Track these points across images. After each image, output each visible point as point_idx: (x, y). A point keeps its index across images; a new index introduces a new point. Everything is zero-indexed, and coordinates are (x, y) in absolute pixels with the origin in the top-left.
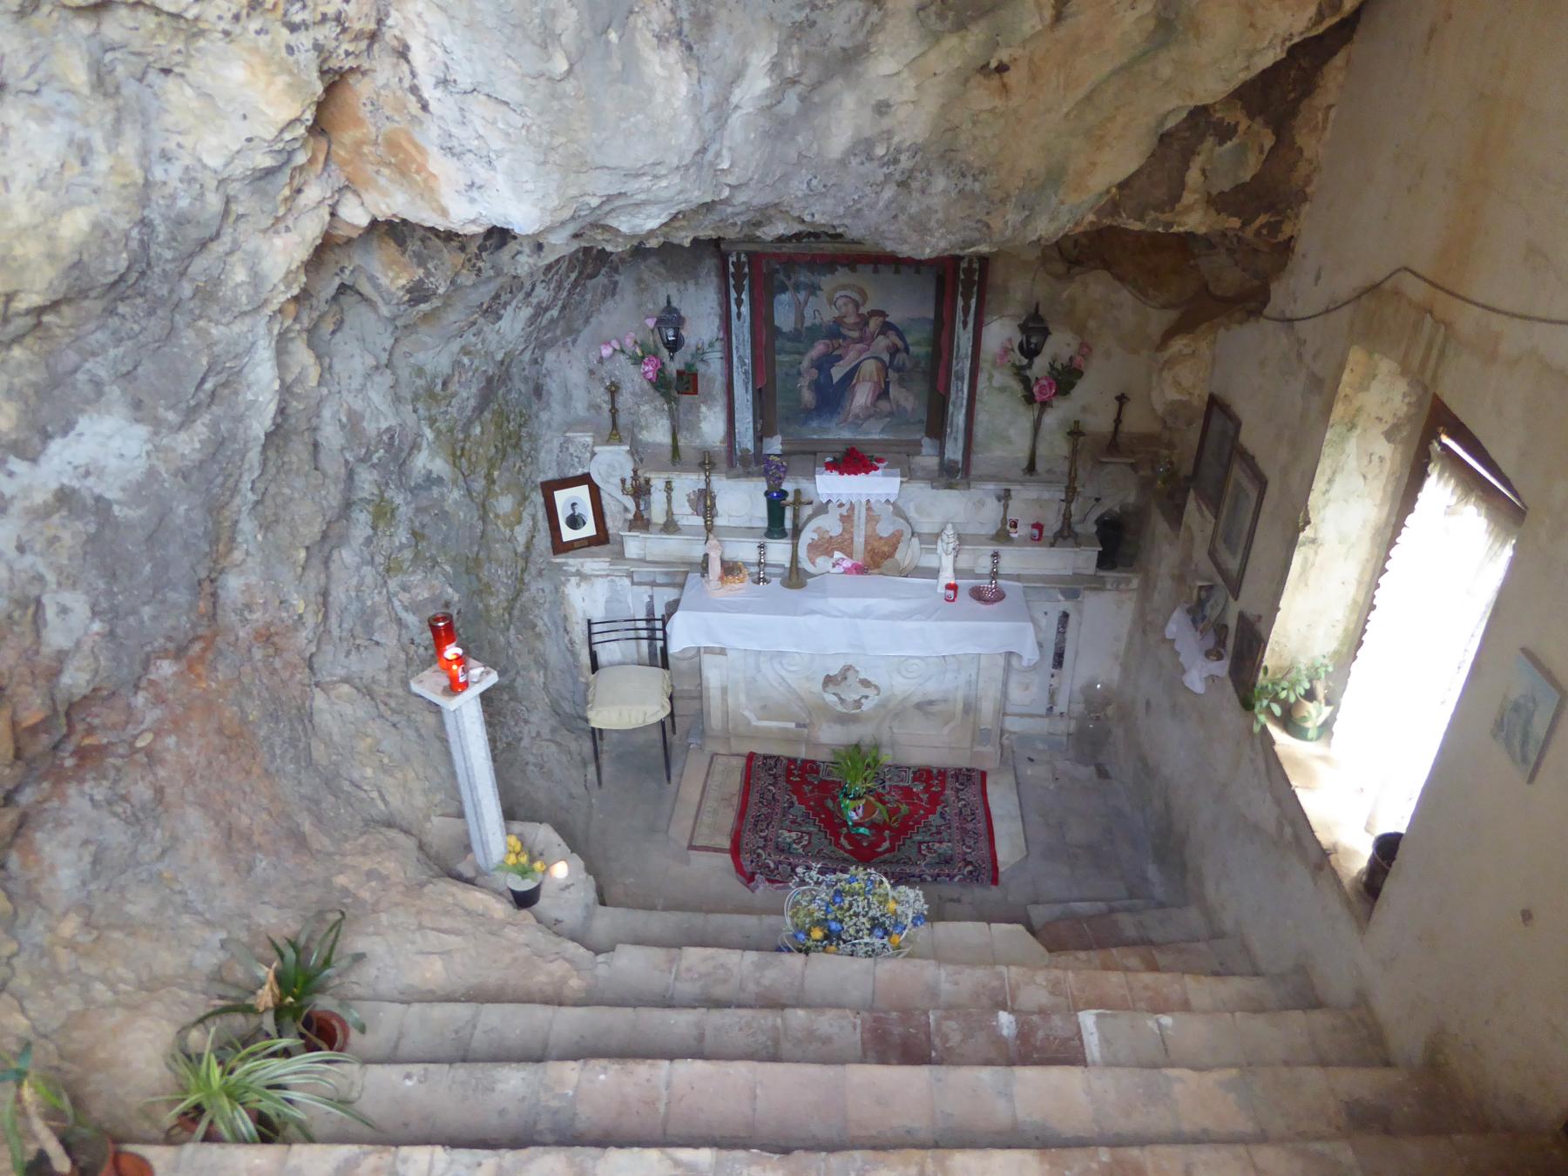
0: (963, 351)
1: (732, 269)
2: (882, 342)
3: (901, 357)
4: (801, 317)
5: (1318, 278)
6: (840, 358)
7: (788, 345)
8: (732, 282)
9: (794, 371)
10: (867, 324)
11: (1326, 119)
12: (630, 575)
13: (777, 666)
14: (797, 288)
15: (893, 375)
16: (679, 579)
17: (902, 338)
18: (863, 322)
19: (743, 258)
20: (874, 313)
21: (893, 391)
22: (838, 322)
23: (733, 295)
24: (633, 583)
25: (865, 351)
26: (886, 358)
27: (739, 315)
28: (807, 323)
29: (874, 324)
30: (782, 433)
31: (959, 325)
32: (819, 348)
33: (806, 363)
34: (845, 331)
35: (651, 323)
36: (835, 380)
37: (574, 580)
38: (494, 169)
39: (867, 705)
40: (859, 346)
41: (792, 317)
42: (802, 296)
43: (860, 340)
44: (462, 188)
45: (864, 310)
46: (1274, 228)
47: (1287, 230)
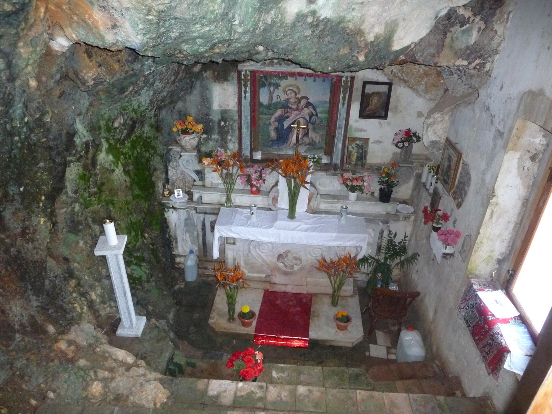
0: (342, 117)
1: (243, 77)
2: (306, 111)
3: (314, 118)
4: (271, 98)
5: (502, 88)
6: (288, 117)
7: (265, 111)
8: (243, 83)
9: (268, 122)
10: (300, 102)
11: (508, 18)
12: (195, 209)
13: (257, 250)
14: (270, 85)
15: (310, 126)
16: (216, 211)
17: (315, 110)
18: (299, 101)
19: (248, 73)
20: (303, 98)
21: (311, 133)
22: (287, 100)
23: (243, 88)
24: (197, 213)
25: (299, 114)
26: (308, 118)
27: (245, 97)
28: (274, 100)
29: (303, 102)
30: (261, 150)
31: (340, 106)
32: (279, 112)
33: (273, 119)
34: (290, 105)
35: (386, 170)
36: (285, 127)
37: (171, 210)
38: (124, 18)
39: (296, 268)
40: (296, 112)
41: (267, 98)
42: (272, 89)
43: (297, 109)
44: (110, 26)
45: (298, 96)
46: (482, 65)
47: (488, 66)
